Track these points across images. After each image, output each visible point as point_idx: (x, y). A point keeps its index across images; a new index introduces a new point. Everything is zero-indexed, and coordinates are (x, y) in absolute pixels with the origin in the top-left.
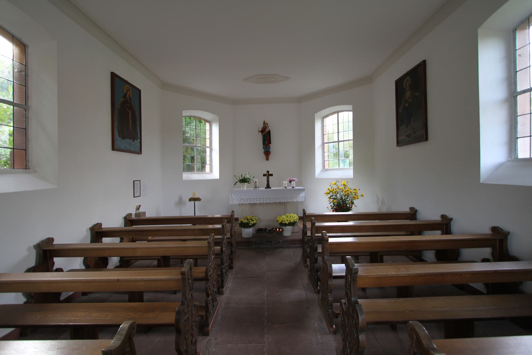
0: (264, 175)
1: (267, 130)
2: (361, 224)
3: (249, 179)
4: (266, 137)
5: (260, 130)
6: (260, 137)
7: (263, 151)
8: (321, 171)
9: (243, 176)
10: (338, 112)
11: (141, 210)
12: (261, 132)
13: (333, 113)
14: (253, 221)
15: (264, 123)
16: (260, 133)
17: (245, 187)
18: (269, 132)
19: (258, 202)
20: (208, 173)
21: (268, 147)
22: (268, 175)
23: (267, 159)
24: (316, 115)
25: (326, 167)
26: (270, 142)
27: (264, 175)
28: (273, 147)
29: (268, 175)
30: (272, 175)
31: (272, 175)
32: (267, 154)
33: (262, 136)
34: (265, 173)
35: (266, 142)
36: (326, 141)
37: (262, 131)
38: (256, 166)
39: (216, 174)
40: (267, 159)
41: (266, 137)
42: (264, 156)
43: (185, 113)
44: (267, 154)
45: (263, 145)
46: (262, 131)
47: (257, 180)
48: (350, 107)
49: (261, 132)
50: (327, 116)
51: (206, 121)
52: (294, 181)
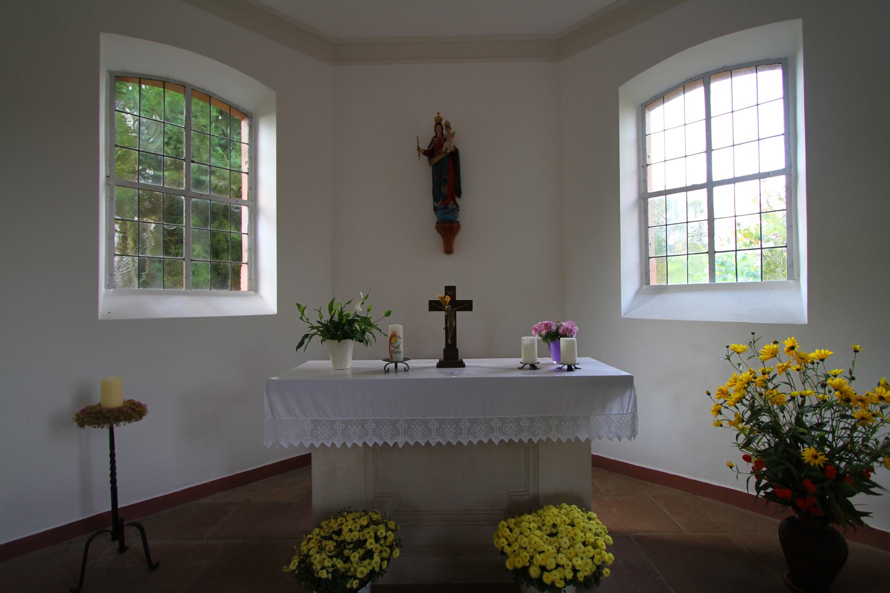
0: (434, 306)
1: (448, 147)
2: (247, 155)
3: (366, 321)
4: (445, 169)
5: (425, 146)
6: (420, 178)
7: (431, 219)
8: (638, 292)
9: (337, 308)
10: (705, 79)
11: (337, 308)
12: (426, 153)
13: (684, 86)
14: (369, 554)
15: (438, 122)
16: (425, 159)
17: (353, 360)
18: (455, 155)
19: (401, 440)
20: (244, 295)
21: (451, 206)
22: (451, 305)
23: (449, 250)
24: (621, 90)
25: (653, 282)
26: (457, 191)
27: (434, 306)
28: (472, 206)
29: (451, 305)
30: (467, 306)
31: (467, 306)
32: (448, 229)
33: (430, 170)
34: (438, 294)
35: (445, 190)
36: (653, 187)
37: (430, 153)
38: (399, 274)
39: (266, 299)
40: (449, 250)
41: (445, 169)
42: (437, 240)
43: (116, 51)
44: (448, 229)
45: (436, 199)
46: (430, 153)
47: (400, 329)
48: (789, 33)
49: (426, 153)
50: (661, 97)
51: (246, 115)
52: (567, 333)
